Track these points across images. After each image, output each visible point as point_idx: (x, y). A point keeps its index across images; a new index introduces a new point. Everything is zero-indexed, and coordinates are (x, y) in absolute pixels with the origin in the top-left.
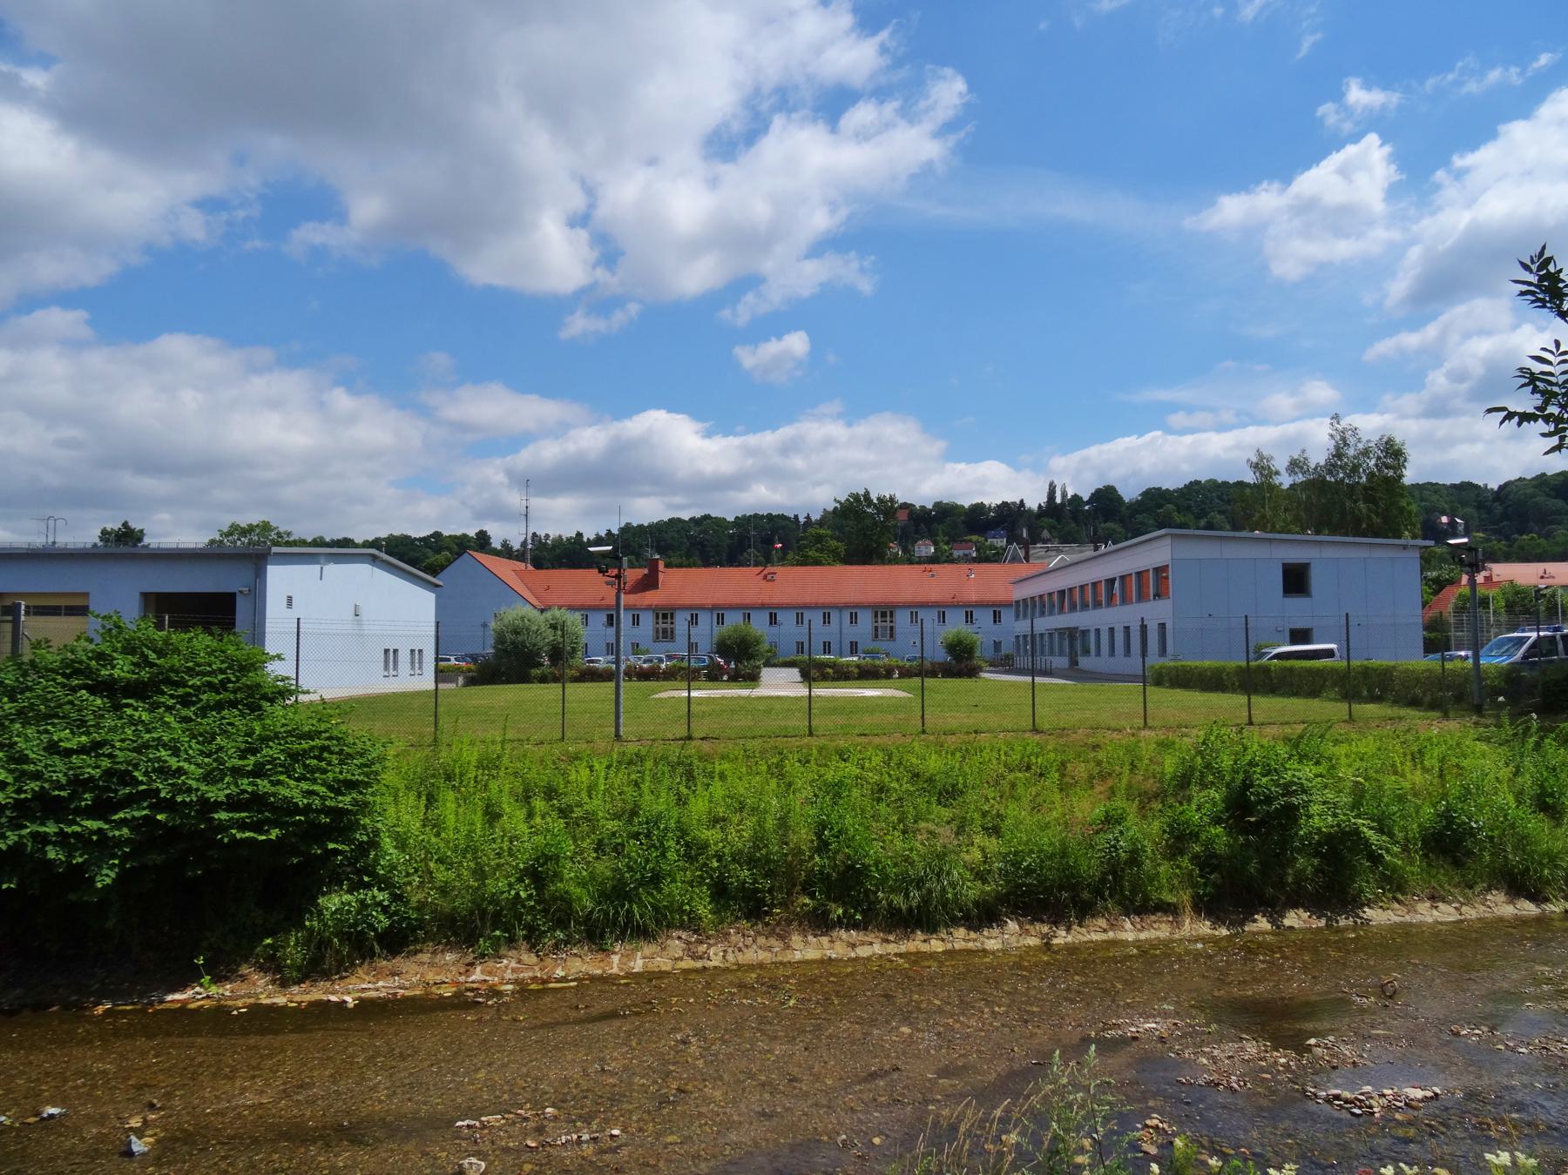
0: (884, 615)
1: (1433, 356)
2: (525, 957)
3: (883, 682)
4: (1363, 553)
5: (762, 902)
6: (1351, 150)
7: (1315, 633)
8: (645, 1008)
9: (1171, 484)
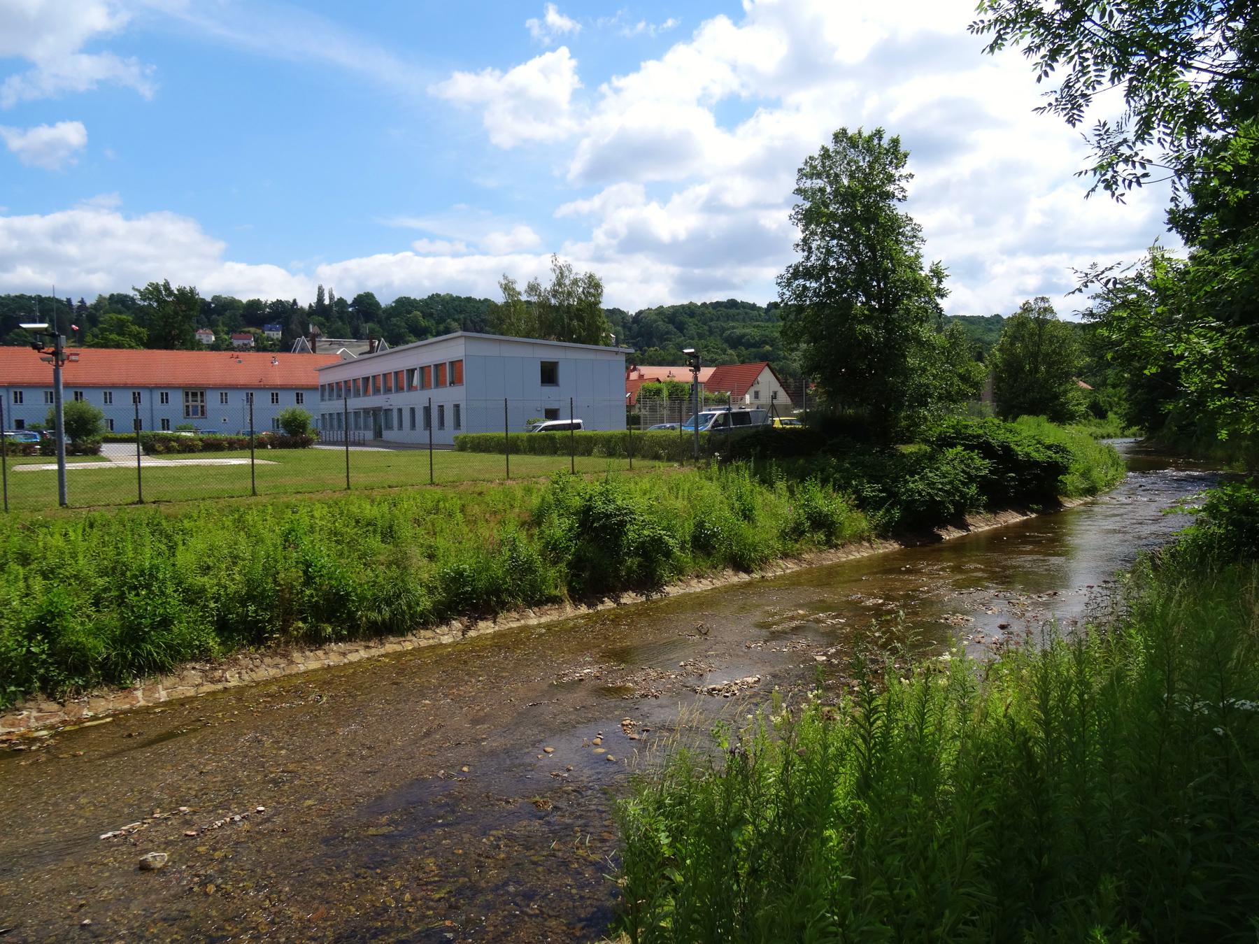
0: (194, 395)
1: (597, 218)
2: (44, 706)
3: (225, 453)
4: (591, 356)
5: (263, 630)
6: (548, 57)
7: (561, 413)
8: (198, 725)
9: (419, 294)
